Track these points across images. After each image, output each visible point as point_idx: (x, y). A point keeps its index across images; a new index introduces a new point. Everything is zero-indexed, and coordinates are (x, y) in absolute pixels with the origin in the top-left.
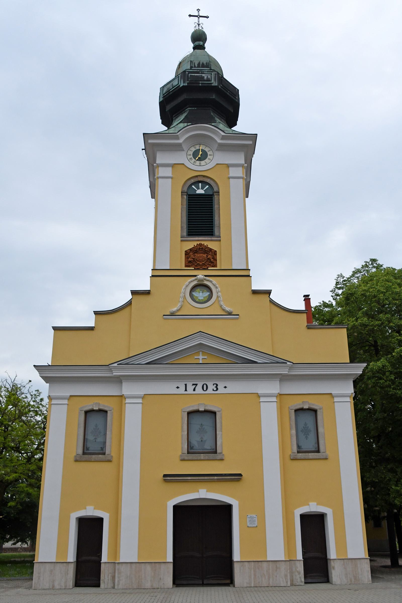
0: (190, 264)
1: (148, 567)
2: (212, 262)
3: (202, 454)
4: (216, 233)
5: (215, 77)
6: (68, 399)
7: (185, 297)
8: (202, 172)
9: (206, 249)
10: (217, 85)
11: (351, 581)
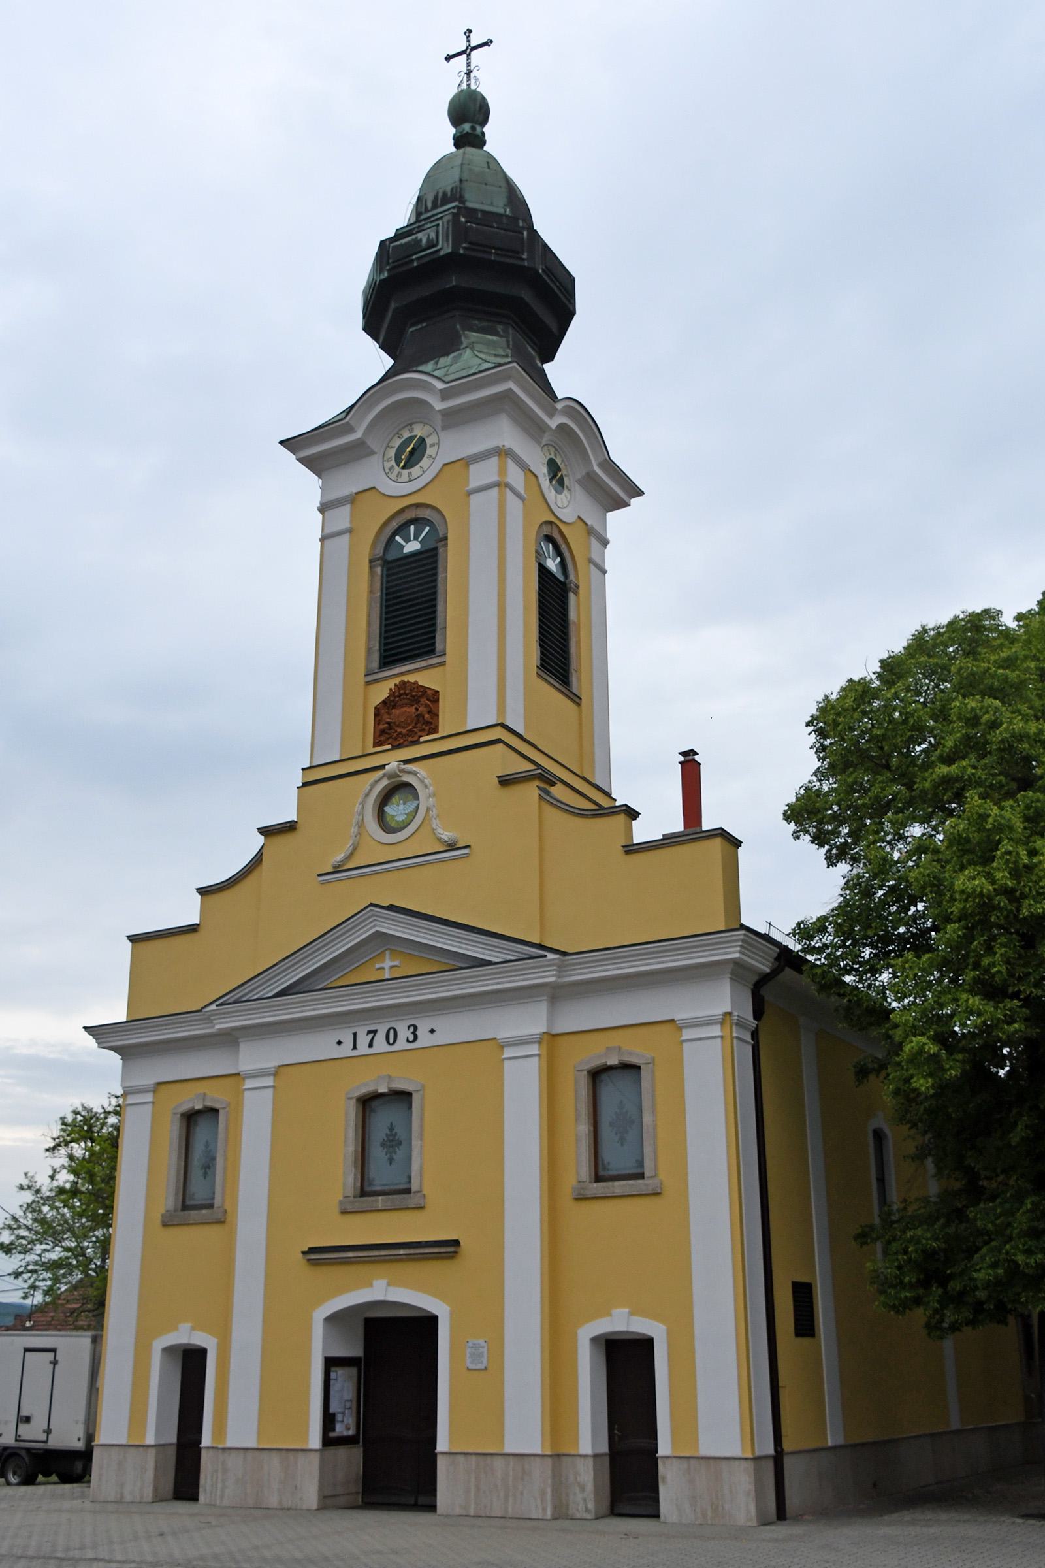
0: (382, 738)
1: (275, 1460)
2: (428, 723)
3: (380, 1198)
4: (439, 647)
5: (448, 228)
6: (154, 1091)
7: (361, 825)
8: (413, 496)
9: (414, 694)
10: (450, 250)
11: (704, 1515)
